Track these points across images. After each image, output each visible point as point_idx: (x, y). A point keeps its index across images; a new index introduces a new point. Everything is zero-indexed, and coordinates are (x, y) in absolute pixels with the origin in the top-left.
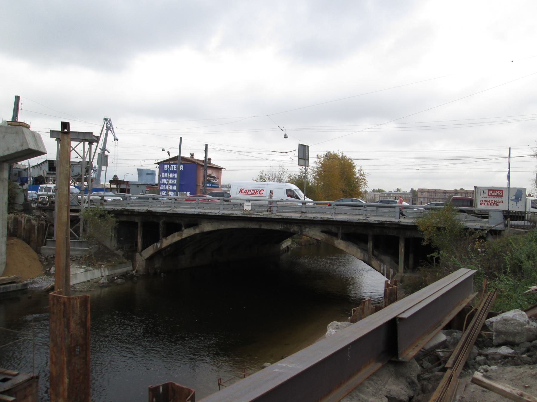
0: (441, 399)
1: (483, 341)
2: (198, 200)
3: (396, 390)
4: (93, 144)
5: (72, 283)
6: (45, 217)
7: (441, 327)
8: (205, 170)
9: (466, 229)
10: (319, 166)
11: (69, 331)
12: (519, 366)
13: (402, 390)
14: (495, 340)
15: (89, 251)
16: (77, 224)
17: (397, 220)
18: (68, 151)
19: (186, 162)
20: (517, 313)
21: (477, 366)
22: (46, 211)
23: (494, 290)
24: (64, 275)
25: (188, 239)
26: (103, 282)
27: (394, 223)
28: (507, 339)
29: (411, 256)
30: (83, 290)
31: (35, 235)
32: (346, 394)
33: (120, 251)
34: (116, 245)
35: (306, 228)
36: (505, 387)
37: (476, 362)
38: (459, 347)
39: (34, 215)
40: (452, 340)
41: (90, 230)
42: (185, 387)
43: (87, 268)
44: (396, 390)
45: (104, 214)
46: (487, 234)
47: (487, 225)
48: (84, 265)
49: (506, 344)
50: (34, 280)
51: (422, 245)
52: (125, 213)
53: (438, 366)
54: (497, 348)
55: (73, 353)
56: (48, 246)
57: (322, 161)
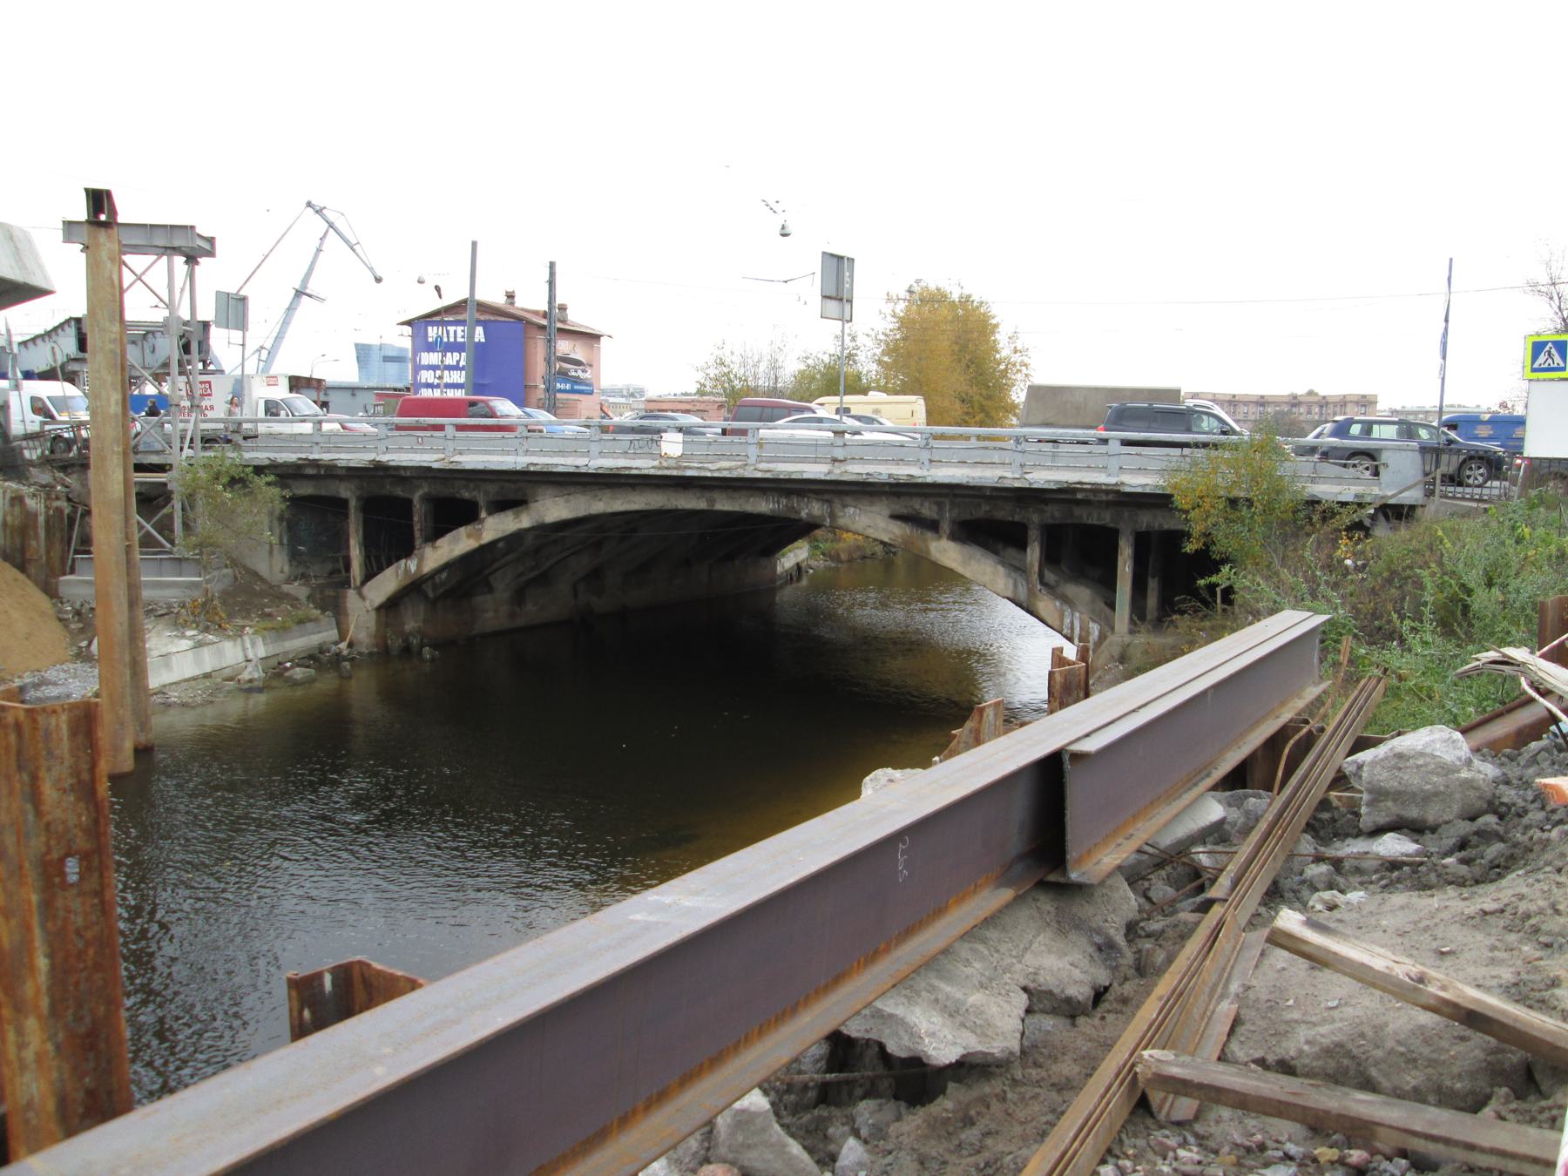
0: (1181, 994)
1: (1334, 820)
2: (524, 428)
3: (1055, 969)
4: (197, 263)
5: (154, 682)
6: (68, 490)
7: (1209, 782)
8: (549, 341)
9: (1313, 502)
10: (891, 326)
11: (39, 813)
12: (1429, 892)
13: (1073, 968)
14: (1368, 818)
15: (204, 585)
16: (165, 506)
17: (1112, 480)
18: (112, 280)
19: (492, 318)
20: (1437, 736)
21: (1305, 892)
22: (69, 471)
23: (1378, 672)
24: (127, 658)
25: (501, 545)
26: (250, 677)
27: (1104, 487)
28: (1403, 813)
29: (1153, 585)
30: (190, 700)
31: (38, 544)
32: (890, 985)
33: (300, 585)
34: (286, 568)
35: (845, 506)
36: (1373, 955)
37: (1303, 882)
38: (1255, 836)
39: (35, 484)
40: (1242, 819)
41: (203, 524)
42: (399, 973)
43: (200, 637)
44: (1055, 969)
45: (242, 475)
46: (1373, 517)
47: (1376, 491)
48: (192, 629)
49: (1397, 826)
50: (42, 677)
51: (1183, 551)
52: (310, 471)
53: (1193, 896)
54: (1371, 840)
55: (57, 880)
56: (79, 575)
57: (902, 311)
